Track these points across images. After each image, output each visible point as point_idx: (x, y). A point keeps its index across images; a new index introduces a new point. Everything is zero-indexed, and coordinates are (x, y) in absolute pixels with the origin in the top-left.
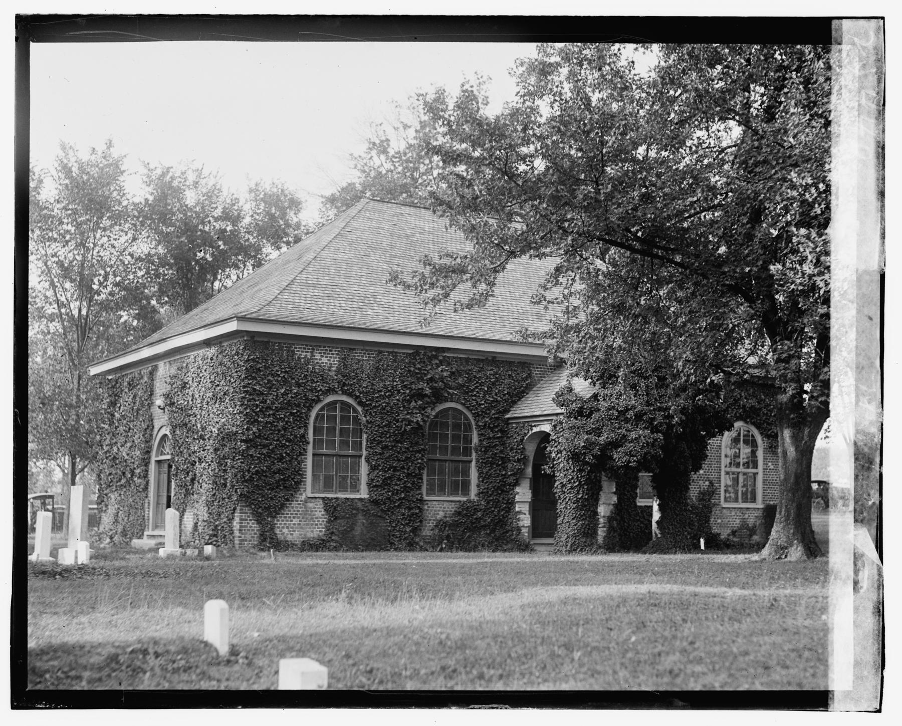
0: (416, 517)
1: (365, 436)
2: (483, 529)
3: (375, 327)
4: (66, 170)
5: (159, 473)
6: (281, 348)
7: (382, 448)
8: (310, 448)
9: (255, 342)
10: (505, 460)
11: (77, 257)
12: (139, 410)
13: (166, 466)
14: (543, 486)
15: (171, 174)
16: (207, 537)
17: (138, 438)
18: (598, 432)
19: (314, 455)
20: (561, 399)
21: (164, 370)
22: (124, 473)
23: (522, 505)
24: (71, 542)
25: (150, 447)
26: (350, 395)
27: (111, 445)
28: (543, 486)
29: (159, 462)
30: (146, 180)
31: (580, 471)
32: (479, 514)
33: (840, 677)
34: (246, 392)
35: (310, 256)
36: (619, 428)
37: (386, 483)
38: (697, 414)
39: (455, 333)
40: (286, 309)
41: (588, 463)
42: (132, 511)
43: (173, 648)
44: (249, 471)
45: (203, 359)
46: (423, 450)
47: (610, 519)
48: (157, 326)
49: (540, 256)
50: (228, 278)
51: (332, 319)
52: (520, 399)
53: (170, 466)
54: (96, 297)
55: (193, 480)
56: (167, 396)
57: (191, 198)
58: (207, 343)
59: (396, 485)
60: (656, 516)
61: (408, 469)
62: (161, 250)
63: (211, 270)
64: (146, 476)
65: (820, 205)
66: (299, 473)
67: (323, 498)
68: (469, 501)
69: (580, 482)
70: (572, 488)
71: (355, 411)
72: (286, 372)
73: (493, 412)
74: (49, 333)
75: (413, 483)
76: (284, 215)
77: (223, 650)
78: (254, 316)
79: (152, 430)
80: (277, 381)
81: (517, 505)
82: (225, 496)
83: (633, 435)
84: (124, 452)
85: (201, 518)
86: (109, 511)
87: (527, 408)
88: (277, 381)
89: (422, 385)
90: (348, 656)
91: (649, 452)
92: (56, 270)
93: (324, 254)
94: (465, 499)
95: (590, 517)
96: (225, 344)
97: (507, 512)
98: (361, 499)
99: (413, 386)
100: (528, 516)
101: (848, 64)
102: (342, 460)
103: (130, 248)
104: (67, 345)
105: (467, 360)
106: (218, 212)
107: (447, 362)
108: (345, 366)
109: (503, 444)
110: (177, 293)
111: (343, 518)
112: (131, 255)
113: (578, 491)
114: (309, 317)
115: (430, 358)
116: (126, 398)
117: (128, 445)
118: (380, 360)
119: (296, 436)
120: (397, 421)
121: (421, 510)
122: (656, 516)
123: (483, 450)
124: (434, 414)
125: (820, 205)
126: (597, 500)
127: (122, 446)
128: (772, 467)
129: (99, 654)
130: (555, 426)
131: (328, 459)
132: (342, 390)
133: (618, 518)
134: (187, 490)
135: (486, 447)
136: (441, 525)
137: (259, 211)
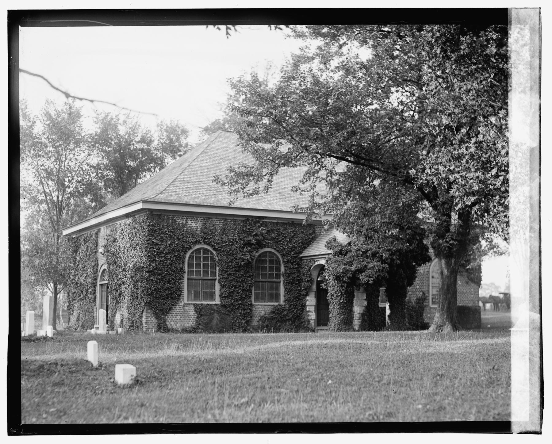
0: (248, 314)
1: (218, 268)
2: (288, 320)
3: (222, 205)
4: (48, 115)
5: (102, 291)
6: (168, 218)
7: (228, 275)
8: (186, 276)
9: (153, 215)
10: (300, 281)
11: (56, 166)
12: (90, 255)
13: (106, 287)
14: (321, 295)
15: (109, 117)
16: (128, 327)
17: (90, 271)
18: (350, 264)
19: (188, 279)
20: (329, 245)
21: (104, 231)
22: (82, 292)
23: (310, 307)
24: (44, 326)
25: (97, 277)
26: (209, 244)
27: (75, 276)
28: (321, 295)
29: (102, 285)
30: (95, 120)
31: (342, 286)
32: (285, 313)
33: (520, 412)
34: (148, 243)
35: (186, 165)
36: (363, 261)
37: (230, 295)
38: (413, 252)
39: (270, 208)
40: (171, 195)
41: (344, 282)
42: (87, 314)
43: (70, 363)
44: (150, 289)
45: (125, 225)
46: (252, 276)
47: (363, 315)
48: (104, 205)
49: (295, 166)
50: (146, 177)
51: (198, 201)
52: (308, 245)
53: (108, 288)
54: (67, 189)
55: (120, 295)
56: (105, 247)
57: (122, 130)
58: (127, 216)
59: (236, 296)
60: (388, 312)
61: (243, 287)
62: (105, 161)
63: (135, 173)
64: (94, 293)
65: (440, 136)
66: (180, 290)
67: (194, 304)
68: (280, 305)
69: (342, 293)
70: (337, 296)
71: (212, 254)
72: (171, 232)
73: (293, 253)
74: (40, 211)
75: (246, 295)
76: (178, 139)
77: (95, 364)
78: (152, 200)
79: (97, 266)
80: (166, 237)
81: (307, 307)
82: (137, 303)
83: (371, 265)
84: (82, 279)
85: (124, 316)
86: (74, 314)
87: (311, 251)
88: (166, 237)
89: (251, 238)
90: (153, 366)
91: (380, 275)
92: (43, 174)
93: (194, 163)
94: (277, 304)
95: (348, 313)
96: (136, 216)
97: (301, 311)
98: (216, 305)
99: (245, 239)
100: (314, 313)
101: (518, 39)
102: (205, 282)
103: (86, 160)
104: (51, 218)
105: (277, 223)
106: (138, 139)
107: (265, 224)
108: (206, 228)
109: (299, 272)
110: (115, 186)
111: (206, 315)
112: (88, 165)
113: (341, 298)
114: (184, 200)
115: (255, 223)
116: (83, 248)
117: (84, 275)
118: (226, 224)
119: (177, 269)
120: (236, 259)
121: (251, 310)
122: (388, 312)
123: (287, 275)
124: (257, 254)
125: (440, 136)
126: (352, 303)
127: (81, 276)
128: (460, 284)
129: (35, 365)
130: (327, 261)
131: (196, 281)
132: (204, 242)
133: (368, 314)
134: (117, 301)
135: (289, 274)
136: (263, 319)
137: (163, 137)
